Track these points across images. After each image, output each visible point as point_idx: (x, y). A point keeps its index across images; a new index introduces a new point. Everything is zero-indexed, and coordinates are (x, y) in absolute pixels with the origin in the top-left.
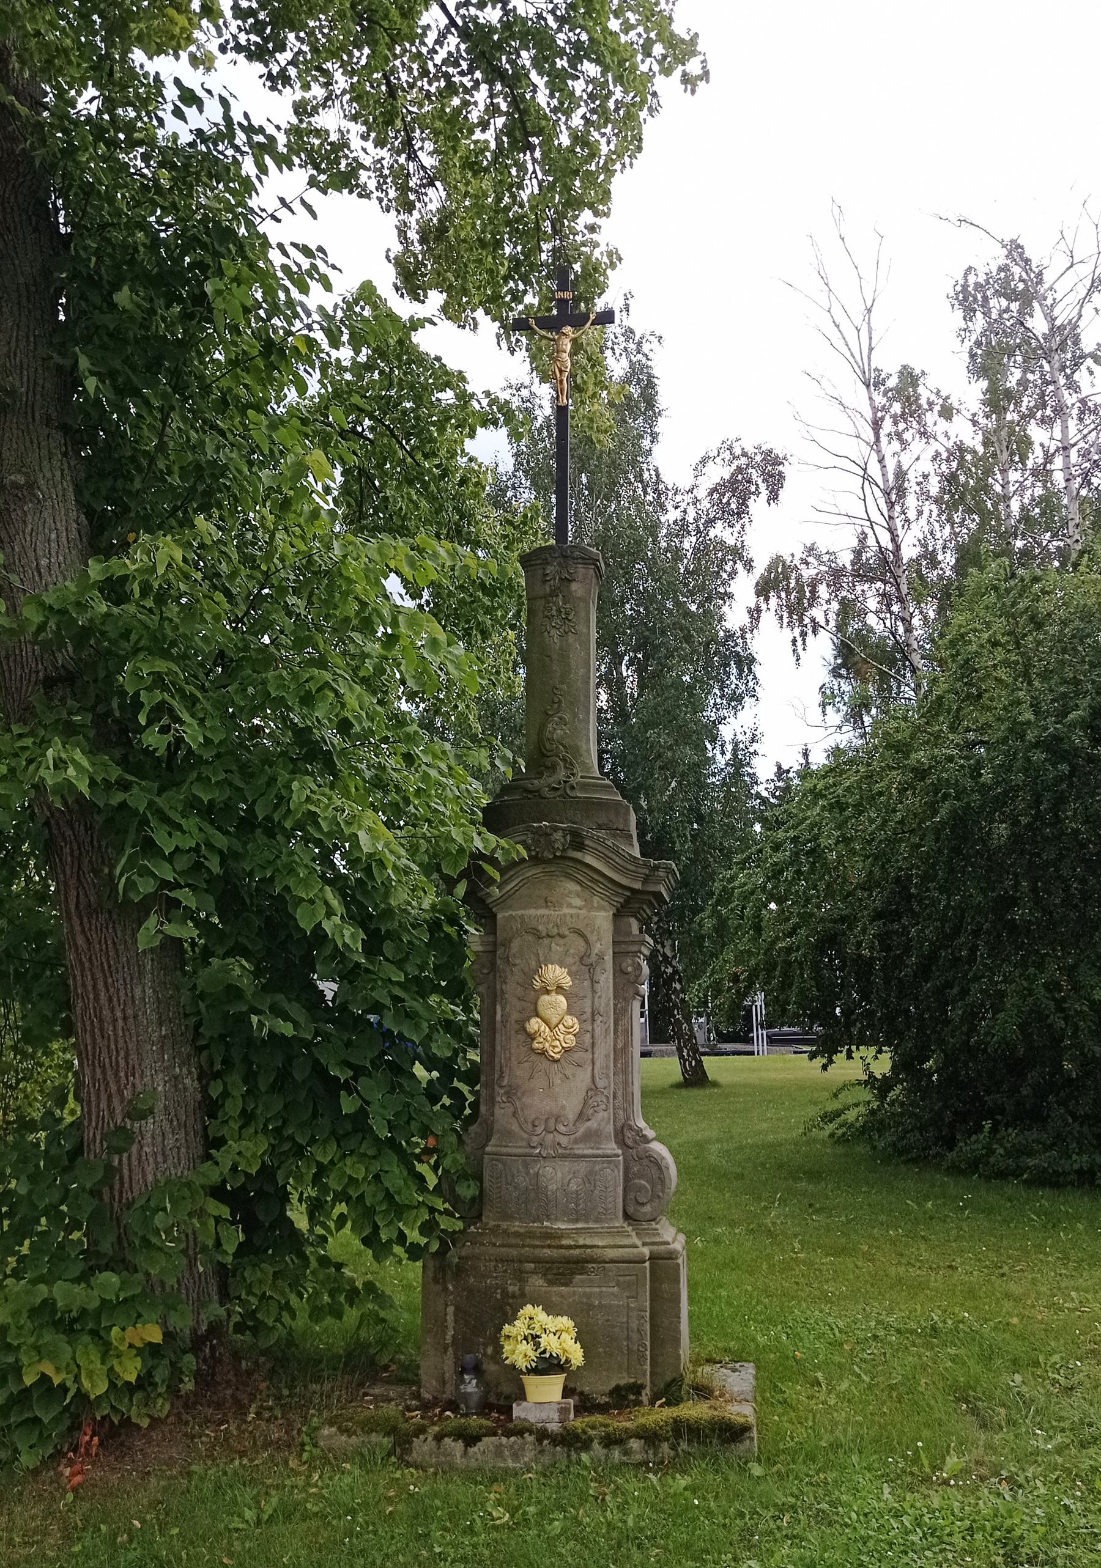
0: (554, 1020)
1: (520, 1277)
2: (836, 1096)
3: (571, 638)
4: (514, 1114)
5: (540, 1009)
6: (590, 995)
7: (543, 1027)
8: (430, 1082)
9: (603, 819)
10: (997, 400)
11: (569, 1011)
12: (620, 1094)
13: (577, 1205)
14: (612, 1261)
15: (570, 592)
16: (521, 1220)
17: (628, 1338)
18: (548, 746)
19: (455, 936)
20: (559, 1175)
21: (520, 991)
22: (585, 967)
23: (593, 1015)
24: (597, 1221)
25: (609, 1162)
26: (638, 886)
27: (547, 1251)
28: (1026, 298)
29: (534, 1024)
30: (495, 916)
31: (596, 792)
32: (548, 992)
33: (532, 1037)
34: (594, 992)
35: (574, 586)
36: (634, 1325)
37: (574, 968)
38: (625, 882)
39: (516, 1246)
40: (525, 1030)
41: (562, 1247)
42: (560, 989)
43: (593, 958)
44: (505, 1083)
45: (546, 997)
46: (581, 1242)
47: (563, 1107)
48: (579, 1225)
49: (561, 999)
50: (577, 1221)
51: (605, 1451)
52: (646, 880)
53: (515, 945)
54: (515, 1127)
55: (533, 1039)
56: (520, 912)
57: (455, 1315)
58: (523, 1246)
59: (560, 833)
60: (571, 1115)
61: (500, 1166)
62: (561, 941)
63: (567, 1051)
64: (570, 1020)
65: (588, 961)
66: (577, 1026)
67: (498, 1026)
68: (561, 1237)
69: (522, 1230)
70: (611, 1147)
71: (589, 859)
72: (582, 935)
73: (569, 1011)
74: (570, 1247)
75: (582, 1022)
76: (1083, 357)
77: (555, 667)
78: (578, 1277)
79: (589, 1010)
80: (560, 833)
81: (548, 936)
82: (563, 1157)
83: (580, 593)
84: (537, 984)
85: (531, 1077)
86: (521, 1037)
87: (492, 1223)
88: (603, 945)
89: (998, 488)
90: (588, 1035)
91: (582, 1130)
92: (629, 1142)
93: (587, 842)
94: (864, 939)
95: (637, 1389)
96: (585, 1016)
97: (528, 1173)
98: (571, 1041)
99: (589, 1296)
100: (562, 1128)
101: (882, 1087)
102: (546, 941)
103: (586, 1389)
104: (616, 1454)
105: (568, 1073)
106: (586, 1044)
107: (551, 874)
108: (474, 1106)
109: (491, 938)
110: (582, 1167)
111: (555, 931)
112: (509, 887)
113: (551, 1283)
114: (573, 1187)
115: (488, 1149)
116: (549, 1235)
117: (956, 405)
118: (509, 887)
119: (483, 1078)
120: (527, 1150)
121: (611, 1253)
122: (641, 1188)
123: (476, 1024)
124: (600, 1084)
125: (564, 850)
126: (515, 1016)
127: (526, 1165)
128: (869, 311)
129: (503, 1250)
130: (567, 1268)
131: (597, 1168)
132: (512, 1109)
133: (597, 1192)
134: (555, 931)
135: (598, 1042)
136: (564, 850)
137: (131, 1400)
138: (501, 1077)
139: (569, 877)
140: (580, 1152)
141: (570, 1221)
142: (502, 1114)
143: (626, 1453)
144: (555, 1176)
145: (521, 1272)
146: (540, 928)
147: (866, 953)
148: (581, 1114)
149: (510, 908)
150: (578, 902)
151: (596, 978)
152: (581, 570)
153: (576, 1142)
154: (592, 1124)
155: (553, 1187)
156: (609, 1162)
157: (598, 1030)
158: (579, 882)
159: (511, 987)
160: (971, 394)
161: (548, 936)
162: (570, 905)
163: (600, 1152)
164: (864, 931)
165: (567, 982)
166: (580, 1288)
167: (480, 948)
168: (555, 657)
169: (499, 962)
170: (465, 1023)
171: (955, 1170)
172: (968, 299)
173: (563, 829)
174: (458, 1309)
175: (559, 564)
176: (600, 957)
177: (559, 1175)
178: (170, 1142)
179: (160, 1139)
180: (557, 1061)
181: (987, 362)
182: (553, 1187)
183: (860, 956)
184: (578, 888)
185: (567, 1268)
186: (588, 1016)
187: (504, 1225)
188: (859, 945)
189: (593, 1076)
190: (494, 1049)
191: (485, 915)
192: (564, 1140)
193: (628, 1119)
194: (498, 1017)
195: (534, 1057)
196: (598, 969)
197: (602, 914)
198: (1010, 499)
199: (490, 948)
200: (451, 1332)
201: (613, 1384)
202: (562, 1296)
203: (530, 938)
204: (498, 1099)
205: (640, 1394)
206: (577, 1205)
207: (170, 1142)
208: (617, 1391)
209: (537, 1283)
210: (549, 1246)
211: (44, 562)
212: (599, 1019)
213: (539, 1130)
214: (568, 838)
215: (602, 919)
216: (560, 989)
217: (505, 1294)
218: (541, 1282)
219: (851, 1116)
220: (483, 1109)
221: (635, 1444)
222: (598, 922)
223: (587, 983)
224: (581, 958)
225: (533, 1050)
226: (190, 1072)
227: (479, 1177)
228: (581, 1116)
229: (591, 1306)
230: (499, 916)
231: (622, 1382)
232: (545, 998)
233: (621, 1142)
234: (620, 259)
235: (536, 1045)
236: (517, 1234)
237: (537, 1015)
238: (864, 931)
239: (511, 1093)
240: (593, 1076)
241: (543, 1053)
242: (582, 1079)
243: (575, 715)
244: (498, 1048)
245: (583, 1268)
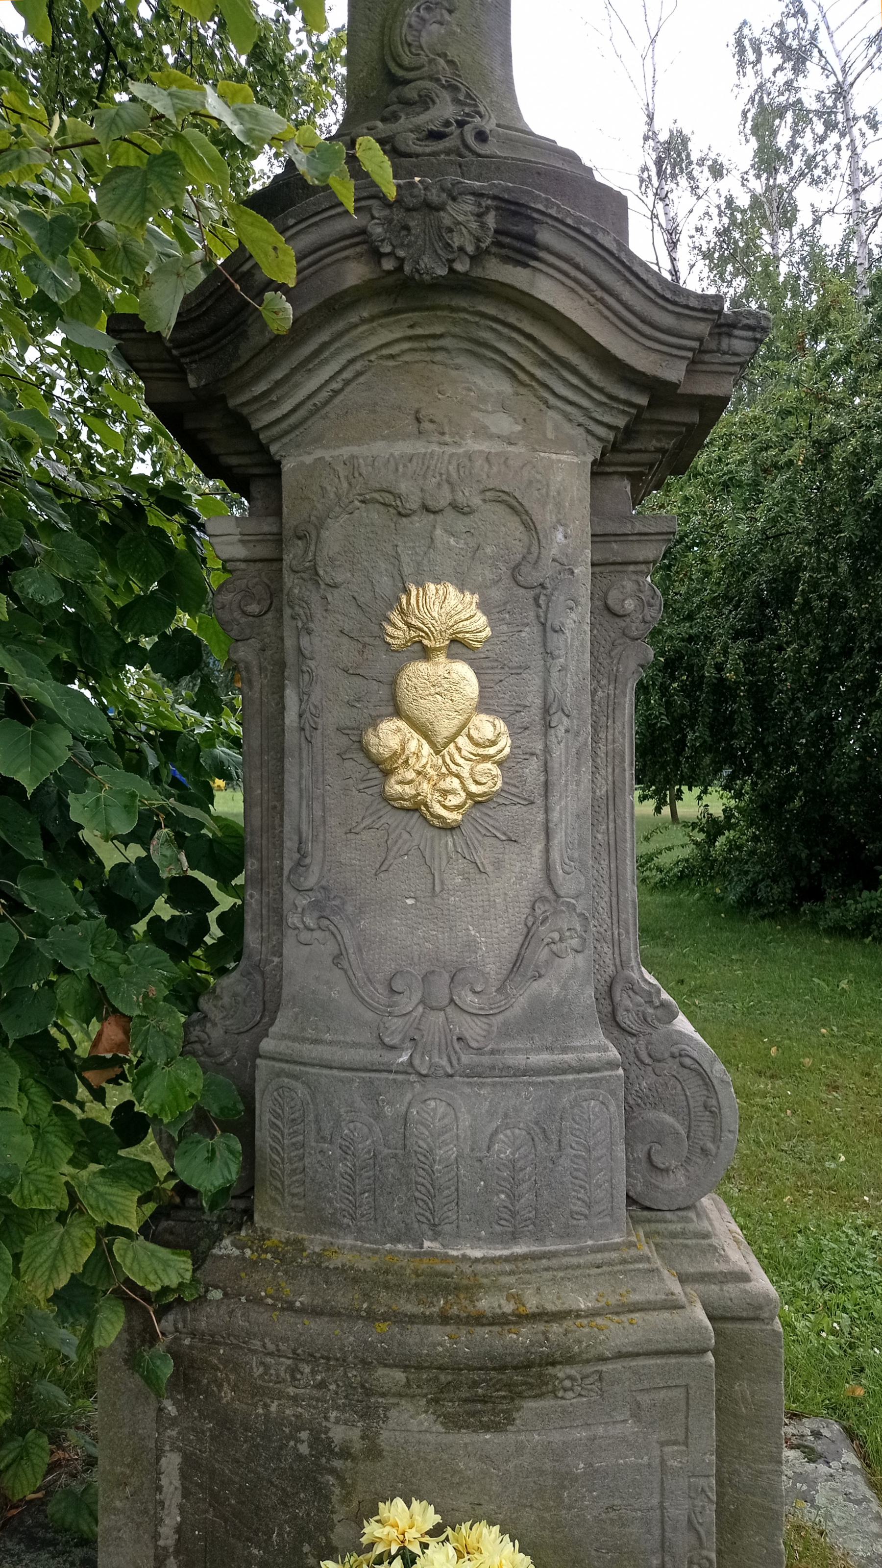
0: (445, 727)
1: (366, 1404)
2: (647, 839)
4: (337, 959)
5: (406, 696)
6: (537, 663)
7: (415, 742)
8: (121, 867)
10: (769, 159)
11: (484, 705)
13: (513, 1197)
14: (620, 1355)
16: (360, 1234)
17: (664, 1546)
18: (406, 60)
19: (178, 541)
20: (466, 1120)
21: (347, 652)
22: (522, 592)
23: (546, 711)
24: (565, 1235)
25: (596, 1084)
26: (674, 372)
27: (439, 1335)
28: (797, 57)
29: (390, 735)
30: (277, 465)
32: (426, 654)
33: (384, 768)
34: (548, 654)
36: (678, 1511)
37: (496, 594)
38: (642, 361)
39: (353, 1315)
40: (364, 750)
41: (479, 1320)
42: (458, 646)
43: (547, 570)
44: (311, 880)
45: (423, 667)
46: (532, 1304)
47: (471, 945)
48: (519, 1249)
49: (463, 671)
50: (514, 1237)
52: (694, 365)
53: (333, 537)
54: (339, 993)
55: (387, 773)
56: (346, 451)
57: (184, 1476)
58: (371, 1317)
59: (468, 206)
60: (493, 968)
61: (301, 1090)
62: (461, 523)
63: (477, 802)
64: (486, 726)
65: (533, 577)
66: (505, 742)
67: (291, 738)
69: (364, 1264)
70: (599, 1046)
71: (547, 290)
72: (517, 509)
73: (484, 705)
74: (500, 1320)
76: (855, 119)
80: (468, 206)
81: (427, 509)
82: (474, 1073)
84: (398, 633)
85: (382, 868)
86: (355, 767)
87: (279, 1234)
88: (568, 536)
89: (767, 249)
90: (534, 764)
91: (520, 1002)
93: (545, 236)
94: (727, 659)
96: (524, 718)
97: (378, 1116)
98: (490, 780)
100: (469, 1000)
101: (713, 828)
102: (420, 522)
105: (484, 857)
106: (527, 784)
107: (429, 344)
108: (233, 922)
109: (267, 526)
111: (444, 497)
112: (312, 384)
113: (452, 1422)
114: (503, 1150)
115: (267, 1045)
117: (726, 164)
118: (312, 384)
119: (251, 864)
120: (376, 1056)
121: (618, 1333)
123: (235, 742)
124: (569, 884)
125: (475, 259)
126: (335, 715)
127: (373, 1095)
128: (653, 41)
129: (314, 1325)
130: (495, 1384)
132: (331, 947)
133: (564, 1162)
134: (444, 497)
135: (560, 781)
136: (475, 259)
138: (300, 864)
139: (479, 350)
140: (519, 1060)
141: (494, 1239)
142: (303, 959)
144: (452, 1123)
145: (369, 1392)
146: (403, 487)
147: (730, 676)
148: (517, 963)
149: (317, 441)
150: (503, 424)
151: (554, 620)
153: (506, 1032)
154: (547, 987)
155: (448, 1152)
156: (596, 1084)
157: (558, 752)
158: (511, 370)
159: (324, 643)
160: (741, 153)
161: (427, 509)
162: (481, 432)
164: (725, 651)
165: (478, 626)
166: (537, 1431)
167: (240, 552)
169: (289, 580)
170: (209, 739)
171: (838, 931)
172: (745, 49)
173: (478, 195)
174: (189, 1466)
176: (566, 568)
177: (466, 1120)
180: (451, 828)
181: (763, 120)
182: (448, 1152)
183: (722, 680)
184: (505, 386)
185: (495, 1384)
186: (535, 713)
187: (315, 1242)
188: (719, 668)
189: (548, 867)
190: (280, 795)
191: (250, 470)
192: (474, 1029)
194: (291, 717)
195: (391, 819)
196: (560, 598)
198: (779, 259)
199: (262, 551)
200: (172, 1519)
202: (486, 1458)
203: (374, 515)
204: (293, 919)
206: (513, 1197)
209: (412, 1425)
210: (445, 1319)
212: (561, 724)
213: (409, 1002)
214: (491, 220)
215: (564, 470)
216: (458, 646)
217: (322, 1445)
218: (426, 1420)
219: (665, 860)
220: (252, 937)
222: (558, 478)
223: (530, 634)
224: (515, 570)
225: (387, 799)
227: (243, 1126)
230: (287, 466)
232: (419, 672)
233: (612, 1022)
235: (394, 788)
236: (352, 1277)
237: (398, 712)
238: (725, 651)
239: (325, 907)
240: (548, 867)
241: (416, 808)
242: (517, 875)
244: (291, 794)
245: (543, 1380)
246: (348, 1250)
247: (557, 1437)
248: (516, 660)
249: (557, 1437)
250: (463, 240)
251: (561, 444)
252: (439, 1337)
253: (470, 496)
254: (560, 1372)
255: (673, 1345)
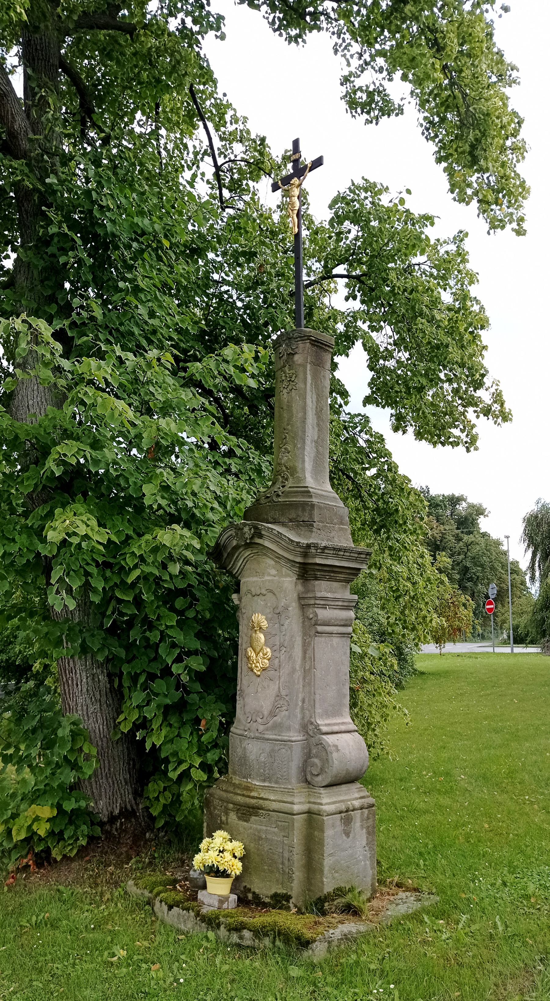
3: (293, 393)
9: (293, 515)
12: (307, 700)
14: (274, 811)
15: (293, 362)
17: (283, 863)
22: (277, 615)
24: (276, 782)
25: (285, 745)
27: (239, 798)
31: (296, 497)
35: (296, 357)
36: (286, 855)
37: (270, 616)
38: (291, 557)
41: (249, 797)
50: (264, 781)
51: (227, 933)
62: (263, 598)
63: (264, 669)
68: (251, 791)
70: (296, 736)
71: (267, 543)
73: (266, 644)
74: (253, 798)
75: (273, 651)
77: (285, 415)
78: (253, 818)
79: (278, 643)
83: (300, 362)
92: (311, 733)
93: (263, 532)
95: (288, 898)
96: (275, 648)
99: (259, 831)
103: (257, 891)
104: (235, 938)
110: (267, 746)
114: (262, 759)
116: (248, 788)
122: (314, 765)
131: (277, 748)
136: (252, 538)
137: (58, 843)
143: (241, 938)
150: (273, 572)
152: (301, 345)
154: (278, 719)
162: (269, 575)
163: (279, 738)
166: (255, 824)
168: (285, 407)
175: (286, 345)
178: (91, 710)
179: (85, 708)
192: (261, 728)
193: (311, 717)
196: (283, 616)
197: (288, 579)
201: (273, 892)
205: (288, 902)
207: (91, 710)
208: (275, 896)
209: (233, 816)
210: (243, 795)
211: (31, 402)
221: (247, 934)
226: (102, 672)
228: (272, 714)
229: (260, 838)
231: (279, 892)
234: (402, 113)
242: (272, 689)
243: (295, 446)
245: (257, 813)
246: (236, 780)
247: (259, 827)
248: (274, 633)
249: (259, 827)
250: (247, 536)
251: (287, 576)
252: (239, 799)
253: (264, 592)
254: (261, 811)
255: (286, 811)
